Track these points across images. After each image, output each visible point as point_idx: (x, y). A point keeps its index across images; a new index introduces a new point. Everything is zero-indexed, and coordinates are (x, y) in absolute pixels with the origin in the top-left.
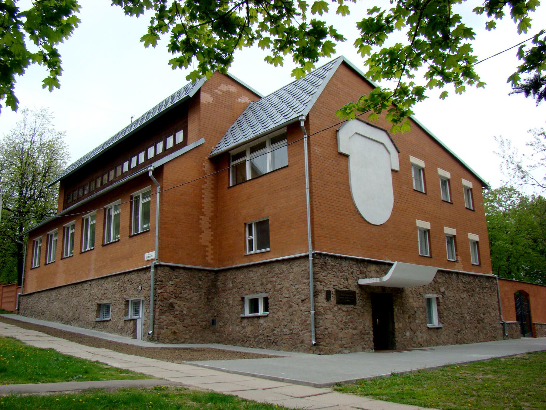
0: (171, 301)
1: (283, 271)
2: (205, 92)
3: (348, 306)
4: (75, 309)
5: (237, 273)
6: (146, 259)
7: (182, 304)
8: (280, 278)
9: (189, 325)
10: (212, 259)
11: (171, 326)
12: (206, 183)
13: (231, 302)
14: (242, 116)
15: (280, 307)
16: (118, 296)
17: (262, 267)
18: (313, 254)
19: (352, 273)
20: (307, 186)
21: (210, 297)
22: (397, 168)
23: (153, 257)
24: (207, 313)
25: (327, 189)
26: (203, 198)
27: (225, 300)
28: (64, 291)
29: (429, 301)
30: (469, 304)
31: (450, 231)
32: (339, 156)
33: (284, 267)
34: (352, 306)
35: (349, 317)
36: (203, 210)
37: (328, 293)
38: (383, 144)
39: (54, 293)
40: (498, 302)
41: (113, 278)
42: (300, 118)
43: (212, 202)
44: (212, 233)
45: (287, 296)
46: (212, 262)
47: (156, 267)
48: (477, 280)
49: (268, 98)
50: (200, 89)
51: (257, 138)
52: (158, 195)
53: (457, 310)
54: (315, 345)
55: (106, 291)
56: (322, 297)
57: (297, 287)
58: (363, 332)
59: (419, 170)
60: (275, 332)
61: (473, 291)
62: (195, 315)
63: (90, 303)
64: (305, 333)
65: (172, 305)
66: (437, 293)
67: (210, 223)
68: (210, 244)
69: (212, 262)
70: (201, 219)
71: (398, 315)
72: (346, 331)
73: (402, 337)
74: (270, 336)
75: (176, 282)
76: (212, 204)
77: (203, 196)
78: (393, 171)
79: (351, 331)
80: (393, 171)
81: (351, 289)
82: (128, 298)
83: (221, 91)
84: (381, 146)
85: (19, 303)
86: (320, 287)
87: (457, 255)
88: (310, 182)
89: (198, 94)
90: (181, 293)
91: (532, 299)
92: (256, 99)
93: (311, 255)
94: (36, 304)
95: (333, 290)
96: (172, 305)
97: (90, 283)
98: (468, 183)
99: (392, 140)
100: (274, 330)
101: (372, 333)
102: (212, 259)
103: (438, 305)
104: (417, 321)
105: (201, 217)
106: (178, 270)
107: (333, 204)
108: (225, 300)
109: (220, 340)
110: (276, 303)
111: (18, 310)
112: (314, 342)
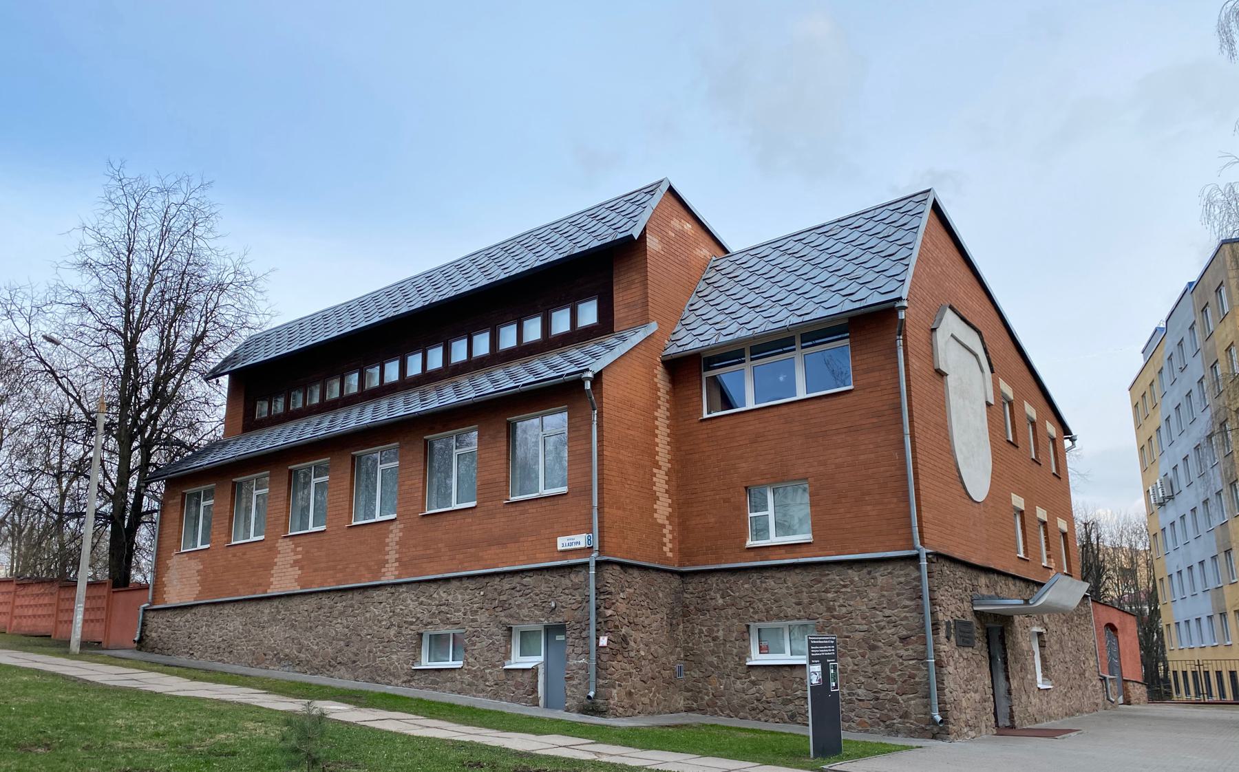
1: (852, 582)
4: (342, 643)
5: (732, 579)
8: (844, 593)
13: (721, 634)
15: (845, 648)
17: (798, 571)
20: (907, 430)
22: (992, 402)
23: (582, 545)
27: (704, 629)
33: (853, 574)
38: (976, 355)
39: (267, 609)
41: (466, 583)
42: (898, 305)
45: (865, 627)
46: (670, 555)
47: (598, 564)
50: (645, 229)
53: (1061, 655)
55: (443, 608)
57: (887, 612)
63: (392, 632)
65: (625, 639)
68: (667, 522)
69: (670, 555)
78: (988, 405)
80: (988, 405)
83: (673, 230)
85: (144, 624)
86: (940, 616)
87: (1049, 557)
89: (643, 235)
92: (720, 253)
96: (625, 639)
98: (1052, 429)
106: (630, 571)
109: (695, 705)
111: (141, 640)
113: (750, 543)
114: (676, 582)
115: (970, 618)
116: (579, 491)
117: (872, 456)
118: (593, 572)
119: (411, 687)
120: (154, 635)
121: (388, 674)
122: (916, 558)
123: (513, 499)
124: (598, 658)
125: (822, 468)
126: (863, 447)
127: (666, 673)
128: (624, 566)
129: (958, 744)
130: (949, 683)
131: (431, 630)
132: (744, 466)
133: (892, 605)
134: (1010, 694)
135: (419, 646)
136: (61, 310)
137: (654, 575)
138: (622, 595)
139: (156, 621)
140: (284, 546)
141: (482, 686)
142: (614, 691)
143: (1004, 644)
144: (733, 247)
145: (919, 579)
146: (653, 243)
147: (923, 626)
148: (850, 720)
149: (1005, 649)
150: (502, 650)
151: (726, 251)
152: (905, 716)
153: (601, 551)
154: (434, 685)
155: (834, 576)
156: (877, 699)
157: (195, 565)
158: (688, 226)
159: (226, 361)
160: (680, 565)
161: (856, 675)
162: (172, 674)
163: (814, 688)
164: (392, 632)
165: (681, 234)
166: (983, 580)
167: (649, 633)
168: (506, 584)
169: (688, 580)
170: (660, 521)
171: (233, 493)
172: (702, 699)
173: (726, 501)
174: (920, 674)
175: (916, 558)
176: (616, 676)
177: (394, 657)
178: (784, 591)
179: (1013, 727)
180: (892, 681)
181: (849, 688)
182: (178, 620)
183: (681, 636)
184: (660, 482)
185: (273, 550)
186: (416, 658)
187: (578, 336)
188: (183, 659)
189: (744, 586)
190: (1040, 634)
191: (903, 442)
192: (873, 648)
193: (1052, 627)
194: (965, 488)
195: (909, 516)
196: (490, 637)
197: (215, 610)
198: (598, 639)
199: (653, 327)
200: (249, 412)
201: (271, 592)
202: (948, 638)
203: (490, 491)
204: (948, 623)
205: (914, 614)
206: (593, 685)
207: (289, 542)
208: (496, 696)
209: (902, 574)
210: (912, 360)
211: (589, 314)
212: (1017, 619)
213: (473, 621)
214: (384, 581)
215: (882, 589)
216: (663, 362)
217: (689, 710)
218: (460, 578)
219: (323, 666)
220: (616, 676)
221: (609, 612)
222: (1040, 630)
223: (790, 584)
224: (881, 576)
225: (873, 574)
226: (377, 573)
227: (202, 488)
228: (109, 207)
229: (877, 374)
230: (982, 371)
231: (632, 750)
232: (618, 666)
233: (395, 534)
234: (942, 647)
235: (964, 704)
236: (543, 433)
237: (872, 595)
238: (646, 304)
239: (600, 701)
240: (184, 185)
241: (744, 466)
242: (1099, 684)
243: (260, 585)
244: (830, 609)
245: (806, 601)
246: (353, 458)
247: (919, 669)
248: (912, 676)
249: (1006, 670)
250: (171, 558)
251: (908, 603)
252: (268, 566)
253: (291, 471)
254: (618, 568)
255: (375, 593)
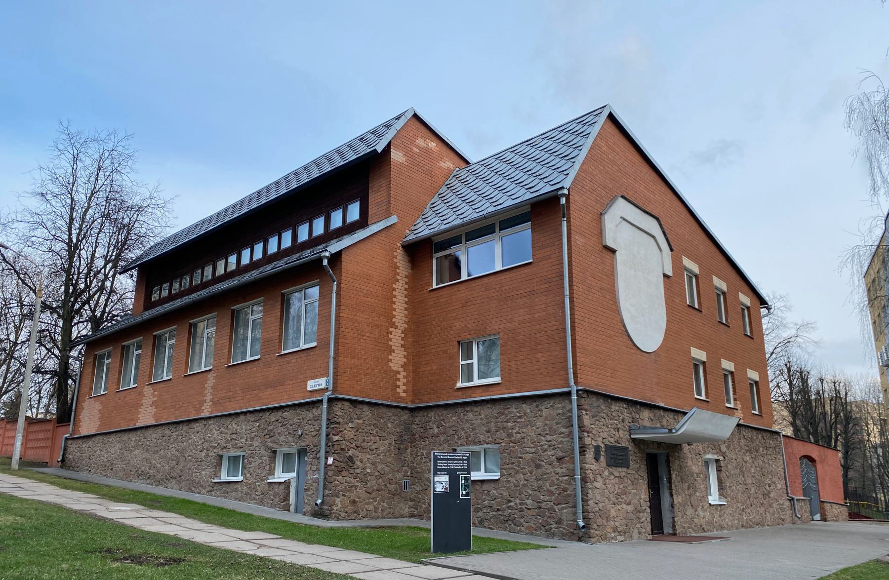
0: (350, 453)
1: (525, 414)
2: (397, 148)
3: (620, 469)
4: (174, 462)
6: (309, 389)
7: (365, 457)
9: (373, 490)
10: (404, 391)
11: (349, 491)
12: (398, 281)
14: (444, 188)
15: (519, 466)
16: (256, 443)
17: (489, 406)
18: (578, 391)
19: (623, 421)
20: (567, 292)
21: (402, 447)
22: (670, 274)
23: (323, 386)
24: (398, 471)
25: (590, 297)
26: (394, 303)
27: (424, 452)
28: (154, 434)
29: (707, 463)
30: (753, 470)
31: (728, 365)
32: (604, 251)
33: (526, 408)
34: (625, 469)
35: (621, 486)
36: (394, 320)
37: (597, 448)
38: (653, 237)
39: (133, 437)
40: (784, 469)
41: (249, 417)
42: (560, 192)
43: (406, 309)
44: (405, 353)
45: (533, 450)
46: (404, 395)
48: (760, 436)
49: (483, 163)
51: (485, 218)
52: (334, 295)
53: (741, 479)
54: (583, 527)
55: (234, 436)
56: (590, 455)
57: (549, 438)
58: (639, 508)
59: (692, 275)
60: (512, 504)
61: (757, 451)
62: (382, 475)
63: (203, 454)
64: (564, 508)
65: (351, 459)
66: (717, 453)
67: (402, 339)
68: (402, 370)
69: (404, 395)
70: (391, 333)
71: (677, 484)
72: (619, 507)
73: (682, 517)
74: (503, 510)
75: (359, 424)
76: (406, 312)
77: (394, 300)
78: (665, 276)
79: (625, 506)
80: (665, 276)
81: (624, 445)
82: (275, 446)
83: (418, 147)
84: (652, 240)
85: (65, 449)
86: (588, 441)
87: (735, 400)
88: (571, 286)
90: (364, 441)
91: (819, 466)
92: (463, 165)
93: (574, 392)
94: (98, 452)
95: (603, 446)
96: (351, 459)
97: (204, 422)
98: (745, 299)
99: (664, 233)
100: (510, 501)
101: (648, 510)
102: (404, 391)
103: (719, 470)
104: (698, 494)
105: (391, 329)
106: (360, 406)
107: (598, 320)
108: (424, 452)
109: (416, 512)
110: (514, 460)
111: (63, 461)
112: (581, 524)
113: (460, 385)
114: (405, 416)
115: (625, 444)
116: (324, 344)
117: (544, 314)
118: (325, 406)
119: (212, 495)
120: (71, 457)
121: (194, 485)
122: (569, 394)
123: (283, 352)
124: (326, 474)
125: (509, 325)
126: (537, 307)
127: (392, 487)
128: (353, 402)
129: (601, 547)
130: (594, 495)
131: (226, 454)
132: (457, 325)
133: (552, 432)
134: (673, 507)
135: (219, 464)
136: (21, 225)
137: (384, 410)
138: (350, 425)
139: (73, 447)
140: (148, 391)
141: (253, 496)
142: (338, 500)
143: (669, 467)
144: (473, 158)
145: (571, 411)
146: (396, 156)
147: (573, 450)
148: (521, 525)
149: (669, 471)
150: (267, 467)
151: (467, 163)
152: (559, 522)
153: (334, 391)
154: (225, 494)
155: (513, 409)
156: (540, 508)
157: (98, 406)
158: (433, 145)
159: (138, 259)
160: (413, 403)
161: (526, 488)
162: (41, 481)
163: (437, 495)
164: (203, 454)
165: (427, 151)
166: (646, 414)
167: (376, 453)
168: (273, 417)
169: (415, 414)
170: (394, 369)
171: (122, 354)
172: (421, 507)
173: (445, 352)
174: (571, 488)
175: (569, 394)
176: (340, 488)
177: (203, 473)
178: (479, 421)
179: (674, 534)
180: (551, 493)
181: (521, 499)
182: (85, 446)
183: (409, 458)
184: (396, 338)
185: (141, 394)
186: (217, 474)
187: (348, 229)
188: (83, 475)
189: (452, 418)
190: (717, 461)
191: (563, 303)
192: (538, 466)
193: (731, 455)
194: (632, 340)
195: (566, 361)
196: (260, 458)
197: (105, 438)
198: (327, 458)
199: (394, 219)
200: (148, 295)
201: (139, 425)
202: (597, 459)
203: (272, 345)
204: (597, 448)
205: (568, 439)
206: (321, 495)
207: (150, 388)
208: (261, 503)
209: (559, 405)
210: (576, 237)
211: (354, 212)
212: (686, 447)
213: (251, 445)
214: (203, 415)
215: (546, 419)
216: (403, 247)
217: (412, 516)
218: (245, 413)
219: (162, 480)
220: (340, 488)
221: (336, 438)
222: (716, 457)
223: (483, 416)
224: (546, 409)
225: (540, 407)
226: (199, 410)
227: (105, 351)
228: (57, 153)
229: (549, 249)
230: (661, 250)
231: (295, 543)
232: (342, 480)
233: (211, 380)
234: (587, 466)
235: (613, 513)
236: (306, 300)
237: (539, 424)
238: (389, 202)
239: (325, 507)
240: (112, 137)
241: (457, 325)
242: (787, 503)
243: (133, 420)
244: (510, 436)
245: (493, 429)
246: (190, 325)
247: (570, 484)
248: (565, 490)
249: (670, 488)
250: (84, 401)
251: (563, 430)
252: (138, 406)
253: (155, 336)
254: (348, 404)
255: (195, 425)
